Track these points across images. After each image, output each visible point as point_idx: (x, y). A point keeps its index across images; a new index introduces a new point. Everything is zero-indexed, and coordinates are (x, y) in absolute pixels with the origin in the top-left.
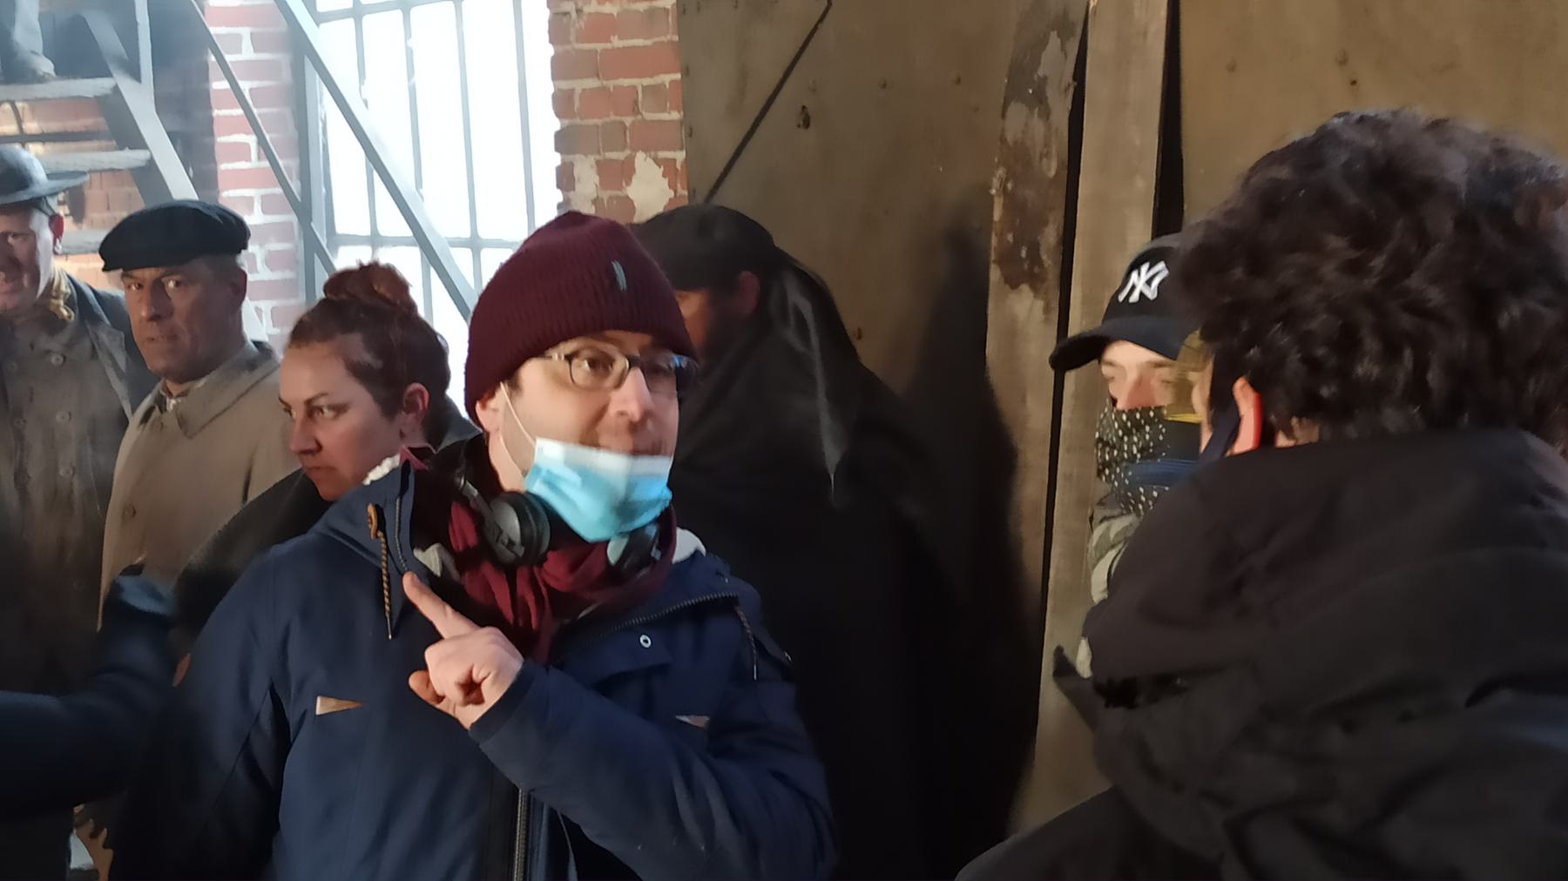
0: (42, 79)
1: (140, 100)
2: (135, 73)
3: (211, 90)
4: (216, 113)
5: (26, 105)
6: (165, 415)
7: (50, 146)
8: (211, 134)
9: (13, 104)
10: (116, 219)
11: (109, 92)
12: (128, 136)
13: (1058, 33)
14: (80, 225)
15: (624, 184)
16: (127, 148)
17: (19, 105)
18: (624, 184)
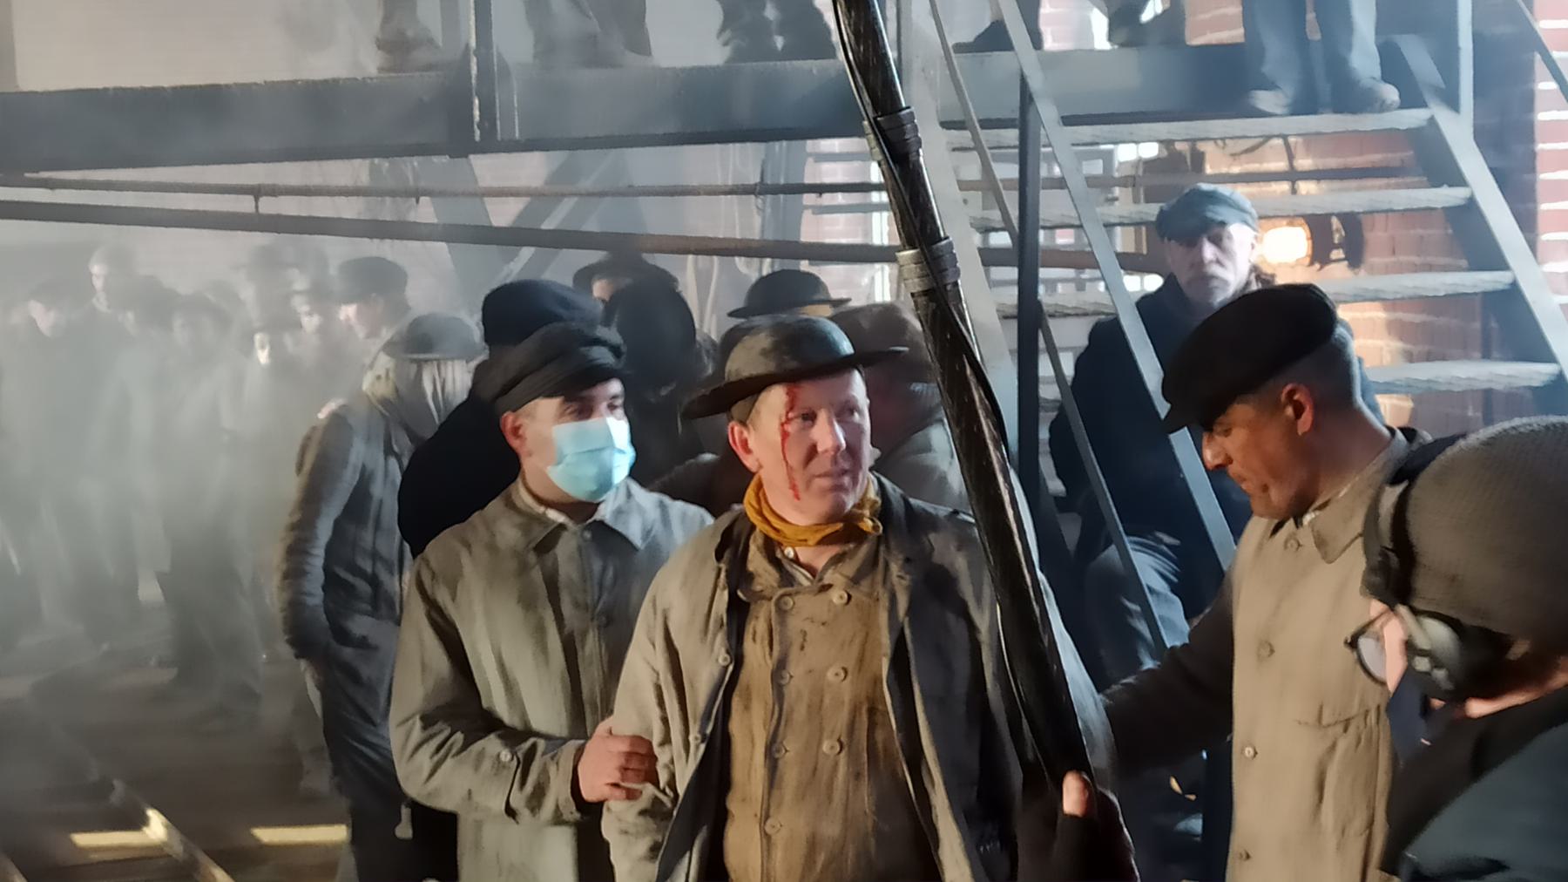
0: (1383, 107)
2: (1453, 103)
3: (1536, 123)
4: (1540, 146)
5: (1300, 140)
6: (1301, 530)
7: (1324, 185)
8: (1532, 169)
9: (1285, 137)
10: (530, 454)
11: (1424, 123)
12: (1443, 171)
14: (1356, 270)
16: (1445, 186)
17: (1292, 140)
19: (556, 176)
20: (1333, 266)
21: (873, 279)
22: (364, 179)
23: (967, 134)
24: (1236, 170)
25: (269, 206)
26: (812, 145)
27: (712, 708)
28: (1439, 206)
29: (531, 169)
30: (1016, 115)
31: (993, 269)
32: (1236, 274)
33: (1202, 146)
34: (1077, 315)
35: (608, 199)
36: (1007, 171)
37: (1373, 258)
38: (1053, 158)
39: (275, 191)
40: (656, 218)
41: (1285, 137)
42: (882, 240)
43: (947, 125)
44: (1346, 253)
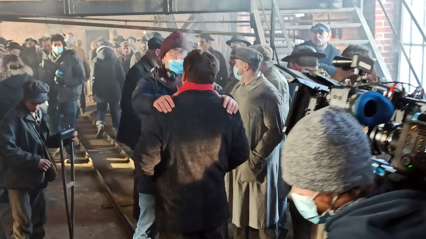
1: (360, 12)
2: (359, 7)
4: (376, 15)
13: (297, 39)
15: (104, 54)
17: (329, 13)
18: (104, 54)
19: (191, 19)
20: (336, 38)
21: (251, 39)
22: (153, 19)
23: (262, 11)
24: (318, 19)
25: (129, 24)
26: (239, 13)
27: (371, 205)
28: (355, 27)
29: (185, 17)
30: (271, 8)
31: (266, 38)
32: (323, 41)
33: (312, 14)
34: (283, 47)
35: (199, 23)
36: (268, 18)
37: (343, 37)
38: (277, 16)
39: (129, 21)
40: (209, 28)
41: (328, 13)
42: (229, 31)
43: (259, 10)
44: (339, 36)
